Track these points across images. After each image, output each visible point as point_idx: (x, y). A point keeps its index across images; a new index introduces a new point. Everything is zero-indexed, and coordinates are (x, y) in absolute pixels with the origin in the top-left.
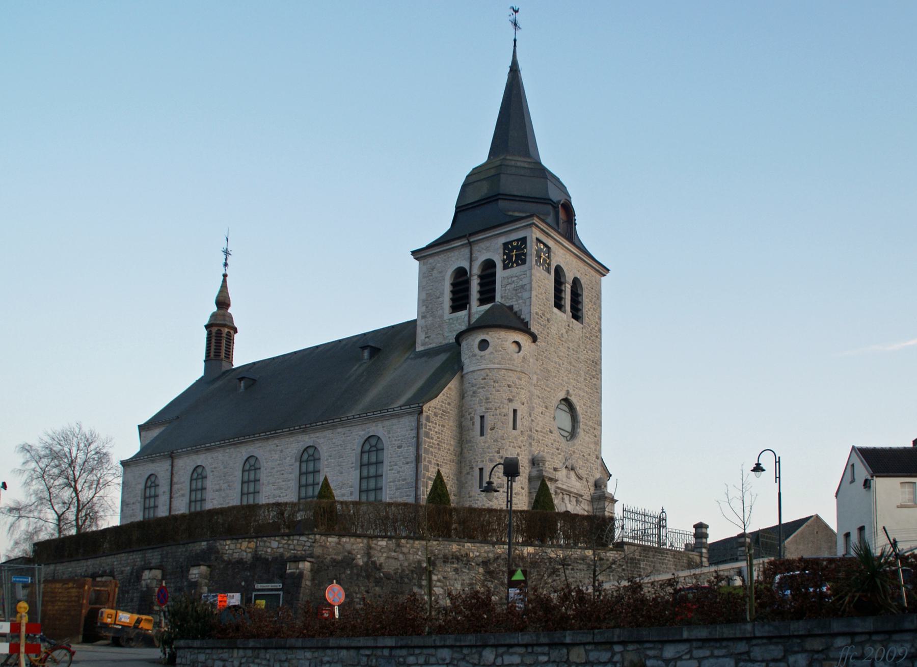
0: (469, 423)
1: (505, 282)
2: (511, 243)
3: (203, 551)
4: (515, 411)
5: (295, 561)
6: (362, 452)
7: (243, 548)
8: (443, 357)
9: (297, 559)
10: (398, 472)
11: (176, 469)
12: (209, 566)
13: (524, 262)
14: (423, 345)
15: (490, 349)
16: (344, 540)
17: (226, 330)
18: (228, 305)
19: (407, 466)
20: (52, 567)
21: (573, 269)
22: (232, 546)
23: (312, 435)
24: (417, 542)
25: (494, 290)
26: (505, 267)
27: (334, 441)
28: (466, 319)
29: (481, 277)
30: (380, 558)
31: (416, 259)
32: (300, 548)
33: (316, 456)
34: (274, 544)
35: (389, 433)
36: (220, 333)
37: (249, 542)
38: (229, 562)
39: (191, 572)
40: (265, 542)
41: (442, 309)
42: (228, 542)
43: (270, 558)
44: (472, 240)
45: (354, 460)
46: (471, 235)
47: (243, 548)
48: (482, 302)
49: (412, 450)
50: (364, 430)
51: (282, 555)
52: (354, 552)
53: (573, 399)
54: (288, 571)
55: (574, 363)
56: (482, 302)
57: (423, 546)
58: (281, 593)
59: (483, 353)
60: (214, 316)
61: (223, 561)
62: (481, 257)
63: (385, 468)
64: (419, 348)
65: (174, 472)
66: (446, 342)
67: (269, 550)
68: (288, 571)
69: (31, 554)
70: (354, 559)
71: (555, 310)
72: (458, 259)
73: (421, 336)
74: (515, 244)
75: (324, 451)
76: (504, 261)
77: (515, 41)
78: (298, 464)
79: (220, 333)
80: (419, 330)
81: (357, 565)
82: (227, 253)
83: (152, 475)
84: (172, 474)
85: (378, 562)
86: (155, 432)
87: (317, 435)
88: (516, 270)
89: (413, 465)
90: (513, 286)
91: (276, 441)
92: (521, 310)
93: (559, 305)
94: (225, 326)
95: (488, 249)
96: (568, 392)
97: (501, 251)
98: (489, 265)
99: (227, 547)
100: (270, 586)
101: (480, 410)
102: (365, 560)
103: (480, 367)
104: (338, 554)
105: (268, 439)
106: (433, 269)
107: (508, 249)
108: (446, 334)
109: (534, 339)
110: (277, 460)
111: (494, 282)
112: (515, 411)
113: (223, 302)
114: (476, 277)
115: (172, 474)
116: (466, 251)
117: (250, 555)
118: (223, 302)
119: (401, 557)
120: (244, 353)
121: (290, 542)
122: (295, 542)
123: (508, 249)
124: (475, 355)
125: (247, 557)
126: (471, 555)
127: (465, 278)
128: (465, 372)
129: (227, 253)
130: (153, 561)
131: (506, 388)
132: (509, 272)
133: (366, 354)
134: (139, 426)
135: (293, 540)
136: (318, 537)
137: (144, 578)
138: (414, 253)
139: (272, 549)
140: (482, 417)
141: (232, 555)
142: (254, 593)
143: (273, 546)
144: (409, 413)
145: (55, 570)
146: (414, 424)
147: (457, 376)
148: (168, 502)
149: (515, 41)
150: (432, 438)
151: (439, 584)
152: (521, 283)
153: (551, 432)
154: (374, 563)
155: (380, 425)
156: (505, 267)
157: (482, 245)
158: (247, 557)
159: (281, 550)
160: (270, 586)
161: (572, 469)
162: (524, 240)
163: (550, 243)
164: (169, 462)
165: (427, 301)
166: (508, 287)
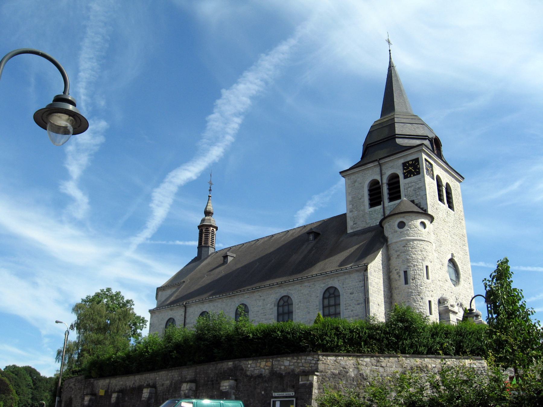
0: (396, 277)
1: (407, 186)
2: (408, 162)
3: (230, 369)
4: (427, 267)
5: (306, 375)
6: (324, 298)
8: (370, 235)
10: (352, 311)
11: (187, 314)
12: (236, 380)
13: (419, 173)
14: (352, 229)
17: (211, 228)
19: (359, 306)
20: (107, 381)
22: (254, 365)
23: (286, 289)
25: (399, 191)
26: (406, 177)
27: (302, 291)
28: (382, 210)
29: (389, 184)
30: (366, 371)
31: (343, 177)
32: (307, 365)
33: (290, 302)
34: (287, 363)
35: (343, 284)
36: (205, 231)
37: (266, 362)
38: (252, 376)
39: (222, 384)
40: (279, 361)
41: (364, 206)
42: (250, 362)
43: (284, 373)
45: (318, 303)
46: (380, 159)
47: (262, 366)
48: (391, 199)
49: (361, 295)
50: (324, 283)
51: (293, 370)
52: (347, 367)
53: (456, 259)
54: (301, 383)
55: (453, 236)
56: (391, 199)
57: (396, 361)
58: (294, 399)
59: (401, 230)
61: (247, 376)
62: (388, 172)
63: (342, 308)
64: (349, 231)
65: (187, 316)
66: (368, 226)
67: (283, 367)
68: (301, 383)
70: (347, 372)
71: (439, 202)
72: (372, 174)
73: (350, 223)
74: (411, 163)
75: (295, 299)
76: (404, 173)
78: (276, 308)
79: (205, 231)
80: (348, 220)
81: (350, 376)
82: (211, 184)
83: (170, 319)
84: (185, 317)
85: (364, 374)
86: (168, 292)
87: (290, 288)
88: (413, 179)
89: (363, 305)
90: (413, 188)
91: (259, 294)
92: (420, 203)
93: (441, 199)
94: (211, 226)
95: (392, 167)
96: (452, 255)
97: (401, 167)
100: (285, 394)
102: (356, 372)
103: (400, 239)
104: (335, 369)
105: (253, 292)
106: (355, 182)
107: (406, 166)
108: (368, 221)
109: (432, 219)
110: (260, 306)
111: (399, 187)
112: (427, 267)
115: (185, 317)
116: (378, 170)
117: (267, 371)
119: (381, 370)
120: (221, 243)
121: (299, 361)
122: (303, 361)
123: (406, 166)
124: (397, 232)
125: (266, 372)
126: (430, 366)
127: (377, 186)
128: (389, 243)
130: (188, 377)
131: (420, 253)
133: (311, 237)
136: (320, 357)
137: (182, 389)
138: (341, 173)
139: (285, 366)
140: (405, 272)
141: (253, 371)
142: (272, 400)
144: (357, 271)
145: (109, 383)
146: (361, 278)
147: (385, 246)
148: (184, 315)
149: (390, 51)
150: (374, 287)
152: (418, 186)
153: (446, 281)
154: (361, 375)
155: (336, 280)
156: (406, 177)
157: (391, 164)
158: (266, 372)
159: (292, 367)
160: (285, 394)
162: (417, 160)
164: (183, 310)
165: (353, 202)
166: (409, 189)
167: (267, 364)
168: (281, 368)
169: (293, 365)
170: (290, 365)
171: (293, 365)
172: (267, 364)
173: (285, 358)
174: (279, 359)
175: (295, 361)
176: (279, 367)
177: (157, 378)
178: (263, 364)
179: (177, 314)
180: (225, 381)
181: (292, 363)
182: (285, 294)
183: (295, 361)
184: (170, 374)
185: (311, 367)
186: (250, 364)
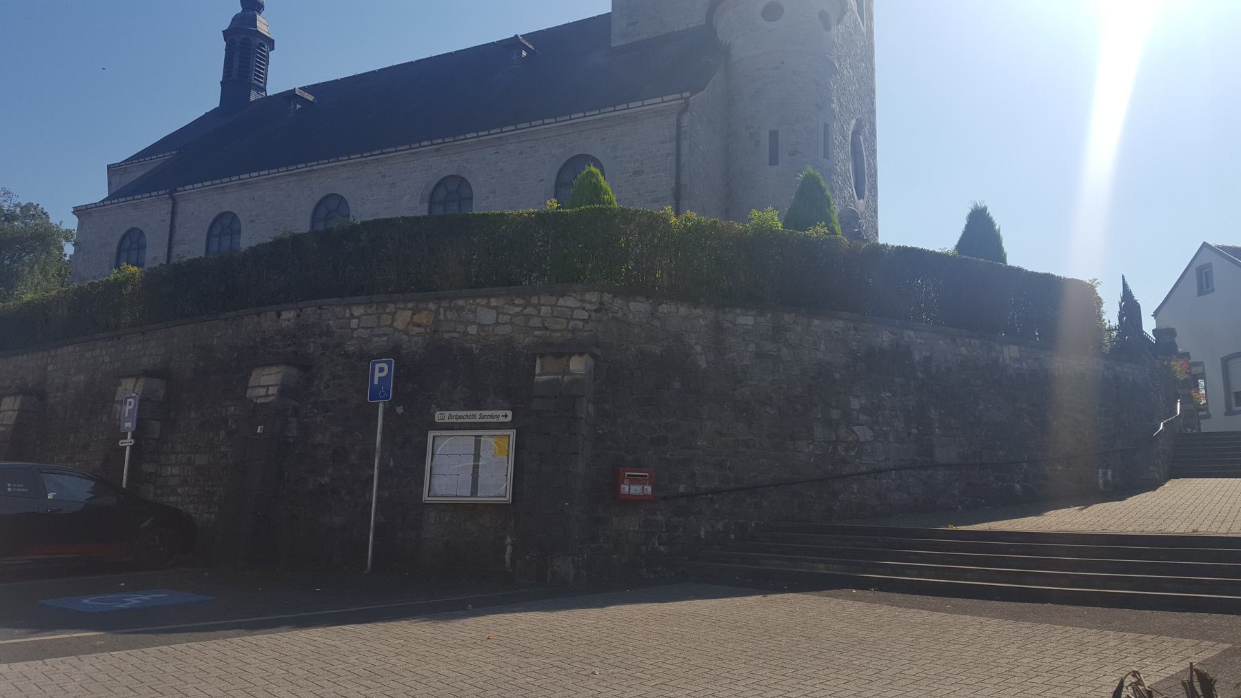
5: (558, 356)
7: (399, 324)
9: (563, 351)
16: (664, 308)
36: (245, 47)
37: (415, 311)
42: (358, 311)
67: (473, 330)
69: (508, 499)
79: (245, 47)
83: (133, 229)
99: (354, 323)
115: (172, 226)
120: (284, 75)
121: (529, 310)
134: (109, 167)
135: (538, 307)
136: (607, 297)
139: (481, 326)
142: (431, 434)
143: (487, 318)
148: (168, 220)
151: (863, 417)
167: (416, 319)
168: (466, 333)
169: (511, 323)
170: (497, 323)
171: (511, 323)
172: (416, 319)
173: (484, 302)
174: (461, 302)
175: (518, 309)
176: (460, 328)
177: (50, 368)
178: (403, 318)
179: (150, 215)
180: (267, 371)
181: (507, 318)
182: (453, 171)
183: (518, 309)
184: (88, 355)
185: (574, 330)
186: (358, 317)
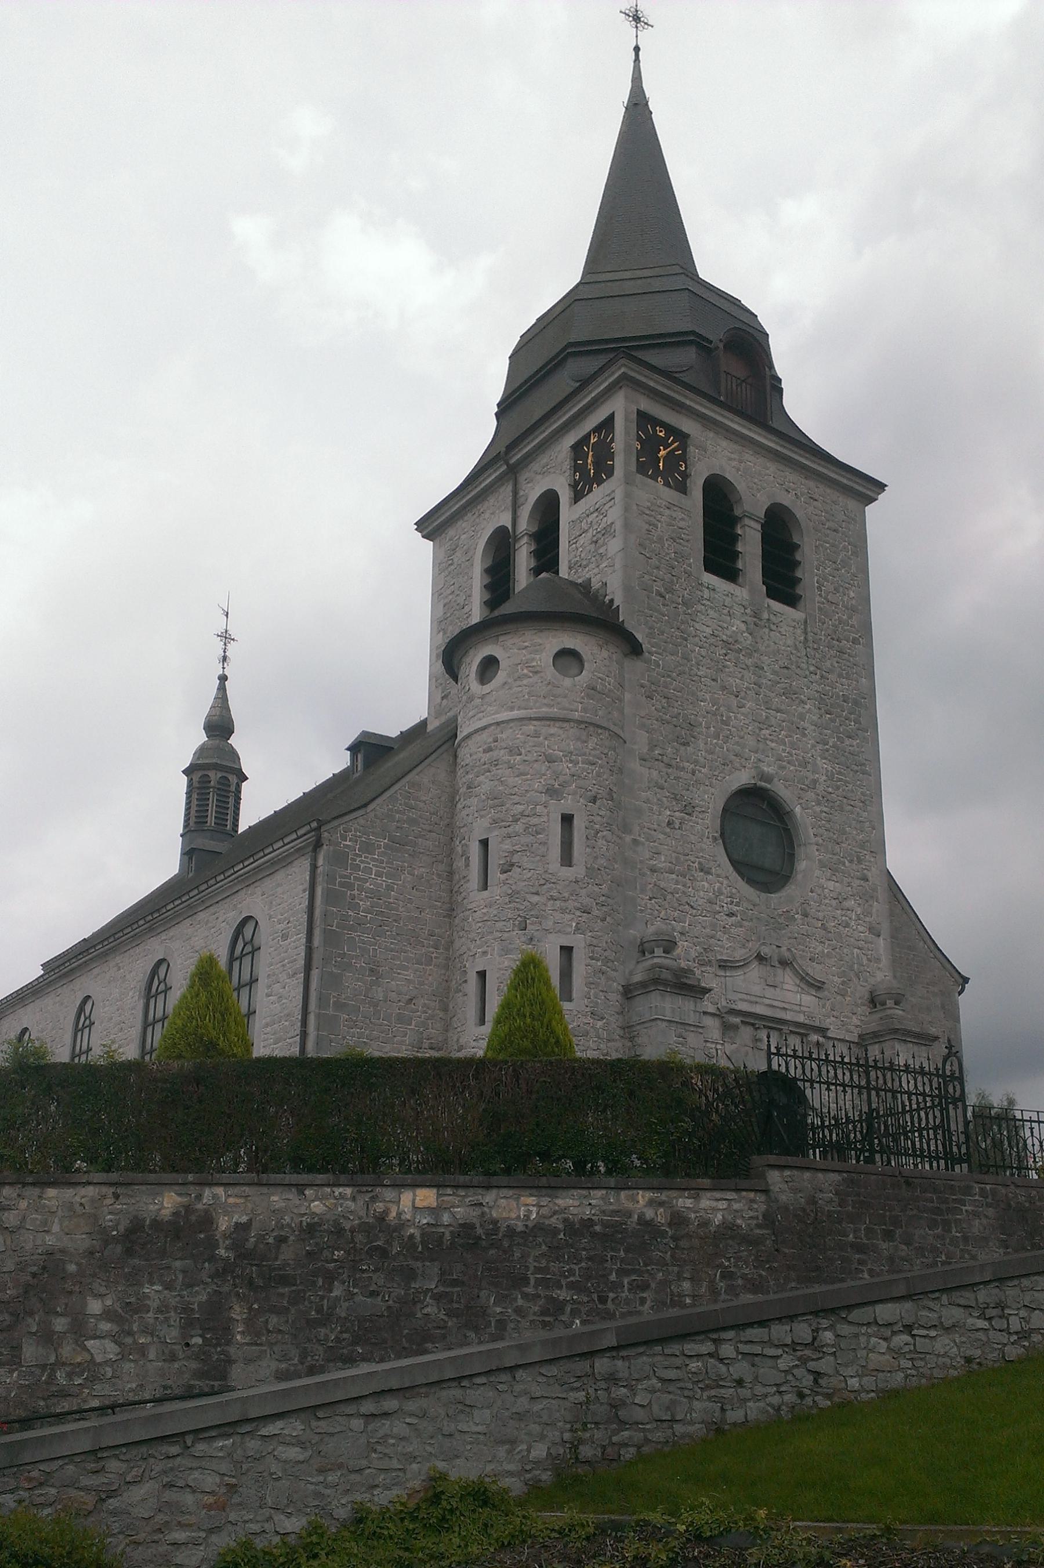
15: (501, 676)
18: (231, 732)
21: (759, 484)
24: (51, 1192)
26: (578, 496)
44: (512, 461)
60: (201, 751)
76: (574, 486)
77: (637, 49)
82: (226, 637)
90: (589, 534)
98: (549, 503)
101: (479, 828)
113: (220, 726)
114: (525, 539)
118: (220, 726)
129: (226, 637)
132: (584, 504)
149: (637, 49)
151: (105, 1326)
156: (578, 496)
161: (784, 963)
163: (686, 425)
